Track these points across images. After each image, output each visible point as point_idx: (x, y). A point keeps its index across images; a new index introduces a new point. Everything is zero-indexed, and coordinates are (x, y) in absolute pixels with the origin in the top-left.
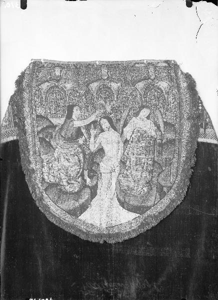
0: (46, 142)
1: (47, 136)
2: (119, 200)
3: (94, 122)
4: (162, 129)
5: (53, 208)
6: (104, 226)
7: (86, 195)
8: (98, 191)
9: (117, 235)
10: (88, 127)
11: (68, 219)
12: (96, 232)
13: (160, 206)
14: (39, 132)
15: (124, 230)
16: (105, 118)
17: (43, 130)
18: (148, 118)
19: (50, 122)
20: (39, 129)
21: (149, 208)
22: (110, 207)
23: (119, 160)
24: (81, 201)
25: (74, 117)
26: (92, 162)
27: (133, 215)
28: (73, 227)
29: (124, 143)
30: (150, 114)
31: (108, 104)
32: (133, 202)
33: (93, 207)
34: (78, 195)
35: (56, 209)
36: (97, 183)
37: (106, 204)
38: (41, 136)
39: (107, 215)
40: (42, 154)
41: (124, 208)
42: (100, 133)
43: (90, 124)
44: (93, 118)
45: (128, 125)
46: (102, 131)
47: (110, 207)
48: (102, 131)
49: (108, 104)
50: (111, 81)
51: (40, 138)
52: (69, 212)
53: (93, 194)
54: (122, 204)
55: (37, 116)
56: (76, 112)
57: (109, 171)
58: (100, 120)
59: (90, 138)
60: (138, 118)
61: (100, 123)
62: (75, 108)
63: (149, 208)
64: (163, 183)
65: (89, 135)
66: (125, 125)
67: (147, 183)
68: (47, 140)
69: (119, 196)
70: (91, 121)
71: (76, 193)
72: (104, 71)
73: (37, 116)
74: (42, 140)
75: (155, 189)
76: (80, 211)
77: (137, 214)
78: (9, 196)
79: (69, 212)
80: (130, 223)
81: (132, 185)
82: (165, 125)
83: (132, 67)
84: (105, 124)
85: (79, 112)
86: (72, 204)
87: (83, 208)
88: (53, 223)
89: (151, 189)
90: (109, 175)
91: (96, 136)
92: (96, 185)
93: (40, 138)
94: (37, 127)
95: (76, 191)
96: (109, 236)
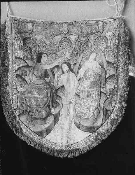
2: (76, 124)
4: (105, 67)
5: (26, 131)
6: (65, 144)
7: (51, 119)
8: (60, 118)
9: (76, 150)
10: (52, 70)
11: (38, 139)
12: (58, 148)
14: (16, 71)
15: (80, 146)
16: (65, 63)
18: (95, 60)
19: (26, 62)
20: (17, 67)
21: (98, 128)
22: (70, 128)
24: (46, 126)
25: (42, 61)
26: (54, 97)
28: (40, 144)
30: (96, 57)
31: (68, 52)
33: (56, 130)
35: (28, 130)
37: (66, 127)
38: (18, 73)
43: (54, 68)
44: (56, 64)
45: (83, 67)
46: (63, 73)
47: (70, 128)
48: (63, 73)
49: (68, 52)
50: (70, 35)
52: (37, 133)
53: (56, 120)
54: (78, 126)
55: (16, 58)
56: (44, 58)
57: (68, 103)
58: (62, 65)
60: (88, 61)
62: (43, 56)
63: (98, 128)
64: (108, 108)
65: (54, 76)
66: (79, 69)
67: (96, 109)
68: (23, 76)
69: (76, 121)
70: (55, 66)
72: (65, 28)
73: (16, 58)
75: (102, 112)
77: (89, 133)
79: (37, 133)
80: (85, 140)
81: (85, 111)
82: (107, 64)
84: (65, 68)
86: (41, 127)
87: (48, 131)
89: (100, 113)
90: (68, 105)
92: (67, 23)
93: (17, 75)
95: (43, 118)
96: (70, 152)
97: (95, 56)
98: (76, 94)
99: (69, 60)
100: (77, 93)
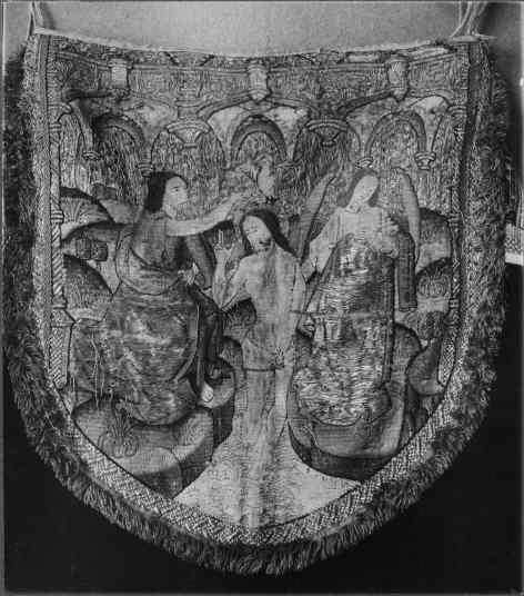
0: (86, 268)
1: (89, 254)
2: (297, 446)
3: (226, 225)
4: (414, 231)
5: (100, 469)
6: (252, 523)
8: (236, 422)
10: (206, 239)
11: (147, 502)
12: (227, 537)
13: (412, 455)
14: (64, 241)
15: (312, 529)
16: (256, 213)
17: (78, 232)
18: (373, 202)
19: (102, 209)
20: (67, 228)
21: (383, 461)
22: (275, 463)
23: (292, 332)
24: (183, 452)
25: (167, 207)
27: (335, 488)
29: (308, 282)
32: (338, 447)
34: (175, 428)
36: (233, 399)
37: (259, 457)
38: (72, 250)
39: (248, 485)
40: (71, 303)
41: (311, 466)
42: (241, 258)
44: (221, 214)
47: (275, 463)
48: (248, 250)
50: (277, 105)
51: (67, 257)
52: (144, 479)
53: (220, 433)
54: (307, 455)
55: (64, 191)
56: (175, 196)
58: (243, 219)
59: (213, 269)
61: (242, 230)
62: (170, 185)
63: (383, 461)
68: (92, 263)
69: (296, 432)
71: (167, 426)
73: (64, 191)
74: (70, 261)
76: (180, 479)
78: (341, 332)
79: (144, 479)
80: (332, 508)
82: (422, 218)
83: (341, 61)
84: (257, 231)
85: (183, 193)
87: (189, 471)
88: (96, 513)
89: (390, 404)
91: (229, 266)
93: (67, 257)
94: (60, 224)
97: (373, 188)
98: (298, 331)
99: (273, 200)
100: (303, 329)
